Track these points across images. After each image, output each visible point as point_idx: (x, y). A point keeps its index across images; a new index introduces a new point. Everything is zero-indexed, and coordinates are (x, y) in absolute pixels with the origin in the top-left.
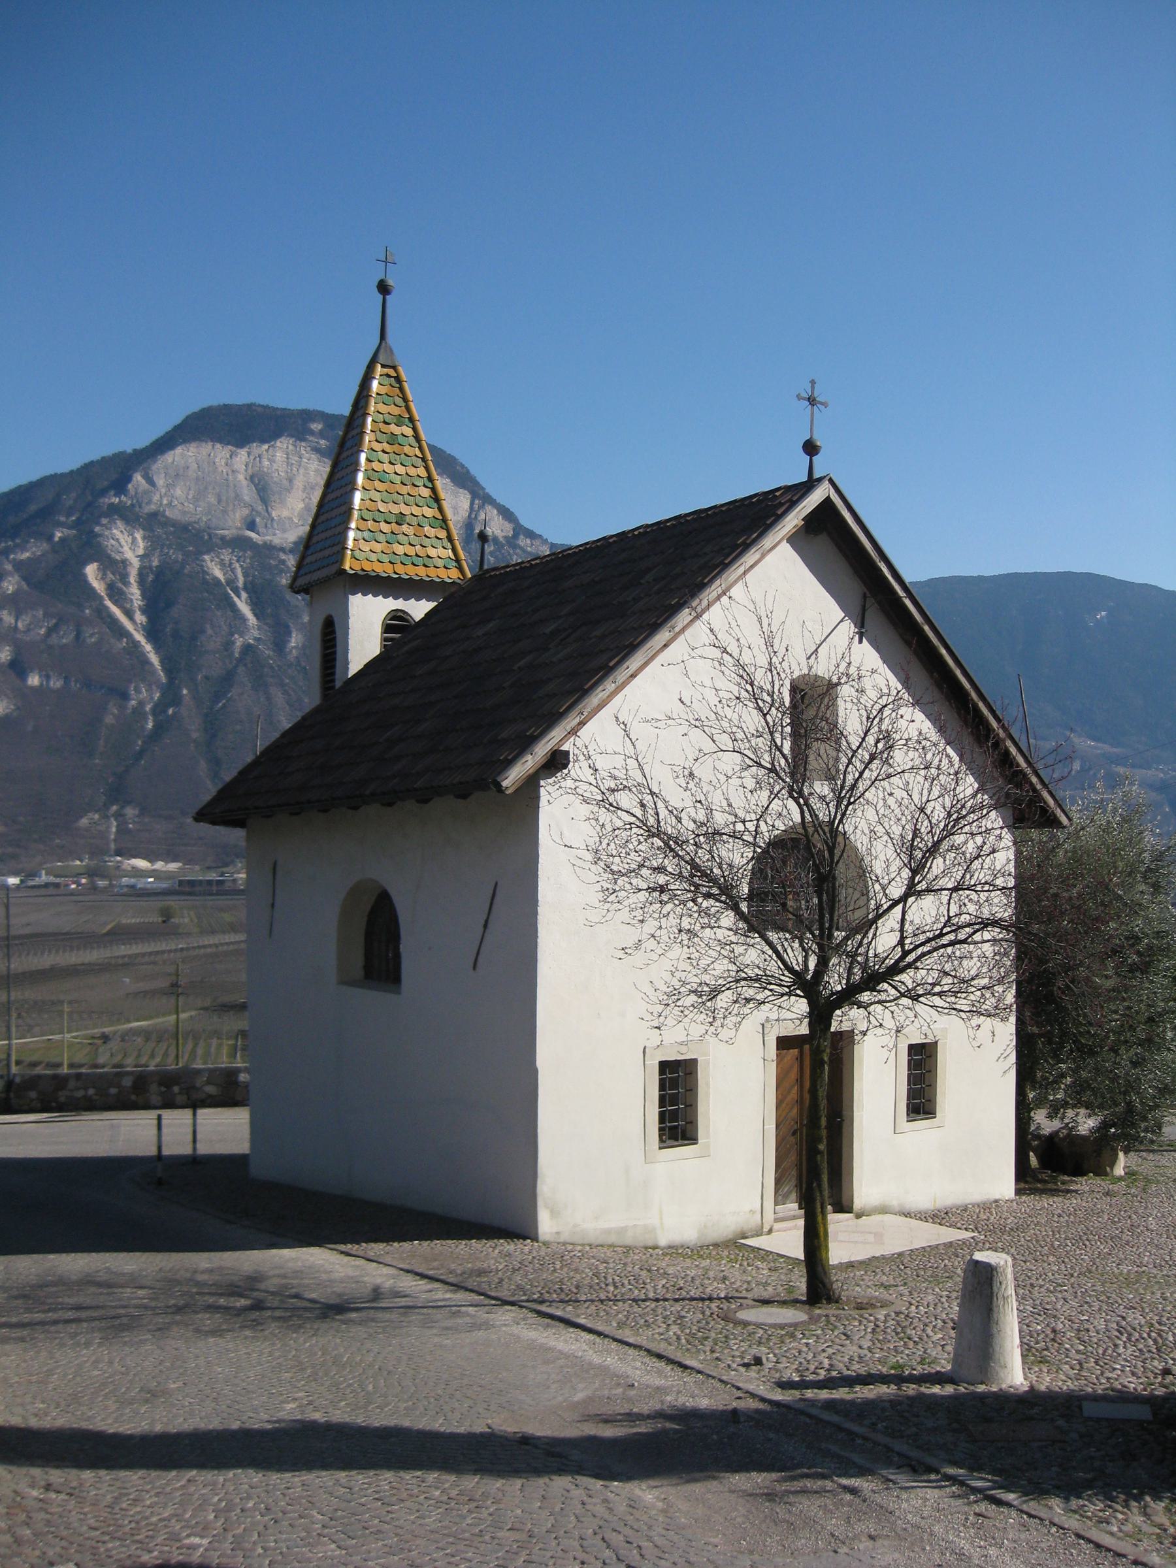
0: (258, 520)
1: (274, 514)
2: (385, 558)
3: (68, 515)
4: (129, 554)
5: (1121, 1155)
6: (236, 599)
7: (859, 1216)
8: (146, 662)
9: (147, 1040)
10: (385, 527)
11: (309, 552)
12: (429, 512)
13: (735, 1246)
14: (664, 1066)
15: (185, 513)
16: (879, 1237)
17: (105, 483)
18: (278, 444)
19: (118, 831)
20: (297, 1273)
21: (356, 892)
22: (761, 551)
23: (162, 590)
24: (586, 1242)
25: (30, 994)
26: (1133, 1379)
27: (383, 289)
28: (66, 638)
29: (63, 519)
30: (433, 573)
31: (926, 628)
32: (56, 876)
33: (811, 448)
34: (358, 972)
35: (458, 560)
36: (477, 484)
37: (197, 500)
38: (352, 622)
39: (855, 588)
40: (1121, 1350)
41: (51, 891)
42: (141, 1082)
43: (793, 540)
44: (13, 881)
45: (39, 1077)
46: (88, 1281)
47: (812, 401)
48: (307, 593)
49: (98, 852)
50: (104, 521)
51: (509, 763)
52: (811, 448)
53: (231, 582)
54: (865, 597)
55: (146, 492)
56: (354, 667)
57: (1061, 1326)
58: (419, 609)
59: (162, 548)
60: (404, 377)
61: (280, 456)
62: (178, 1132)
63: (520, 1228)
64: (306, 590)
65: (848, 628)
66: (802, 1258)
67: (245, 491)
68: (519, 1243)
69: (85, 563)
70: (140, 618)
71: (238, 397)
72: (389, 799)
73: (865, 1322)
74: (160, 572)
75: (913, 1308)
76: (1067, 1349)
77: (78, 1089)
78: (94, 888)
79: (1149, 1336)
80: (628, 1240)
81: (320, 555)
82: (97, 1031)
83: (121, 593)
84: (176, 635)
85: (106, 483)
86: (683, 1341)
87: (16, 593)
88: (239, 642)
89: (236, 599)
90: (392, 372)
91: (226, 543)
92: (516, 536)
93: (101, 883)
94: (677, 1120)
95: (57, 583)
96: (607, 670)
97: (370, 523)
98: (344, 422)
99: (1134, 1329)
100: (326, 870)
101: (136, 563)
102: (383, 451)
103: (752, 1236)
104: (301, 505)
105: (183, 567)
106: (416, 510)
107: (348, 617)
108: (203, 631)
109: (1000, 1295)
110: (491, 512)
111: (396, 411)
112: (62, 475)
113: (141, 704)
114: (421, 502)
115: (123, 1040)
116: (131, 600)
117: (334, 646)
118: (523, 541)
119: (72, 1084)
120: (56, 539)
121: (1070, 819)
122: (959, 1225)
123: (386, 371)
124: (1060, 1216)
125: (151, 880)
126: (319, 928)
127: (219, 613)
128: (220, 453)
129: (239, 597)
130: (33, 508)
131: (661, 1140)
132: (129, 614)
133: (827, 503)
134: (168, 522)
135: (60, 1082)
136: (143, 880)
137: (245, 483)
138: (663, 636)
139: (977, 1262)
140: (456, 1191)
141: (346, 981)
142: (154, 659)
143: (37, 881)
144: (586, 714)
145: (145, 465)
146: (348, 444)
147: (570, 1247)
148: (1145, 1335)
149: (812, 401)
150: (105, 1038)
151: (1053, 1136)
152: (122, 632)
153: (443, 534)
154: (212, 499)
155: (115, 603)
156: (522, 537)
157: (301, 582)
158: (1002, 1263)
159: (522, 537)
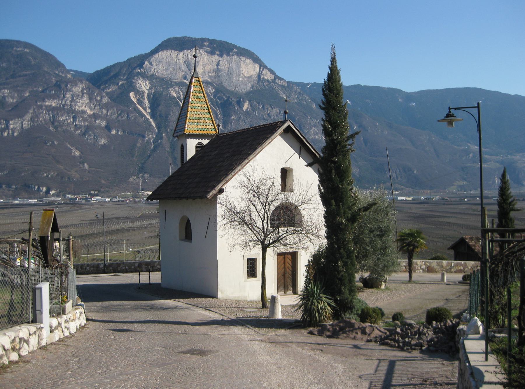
2: (196, 129)
3: (124, 76)
4: (144, 89)
8: (151, 125)
9: (152, 252)
10: (196, 121)
12: (207, 116)
14: (249, 260)
15: (162, 74)
17: (136, 65)
20: (162, 304)
21: (183, 218)
25: (114, 237)
28: (124, 117)
29: (122, 77)
30: (208, 132)
32: (122, 198)
34: (184, 237)
35: (215, 129)
36: (261, 62)
39: (298, 145)
41: (121, 202)
42: (140, 264)
43: (281, 135)
44: (108, 200)
45: (113, 263)
46: (118, 305)
49: (136, 189)
50: (136, 78)
51: (209, 192)
53: (179, 97)
55: (150, 68)
56: (188, 159)
58: (205, 142)
62: (144, 278)
63: (213, 295)
65: (297, 155)
67: (183, 66)
68: (213, 299)
69: (130, 93)
70: (148, 110)
71: (180, 34)
72: (187, 198)
74: (155, 95)
78: (135, 202)
80: (240, 299)
82: (136, 250)
83: (142, 102)
84: (160, 116)
85: (136, 65)
87: (107, 103)
90: (197, 79)
91: (177, 84)
92: (275, 79)
93: (137, 200)
95: (121, 99)
96: (233, 170)
100: (177, 212)
101: (147, 92)
104: (202, 71)
105: (162, 93)
106: (204, 116)
108: (170, 114)
110: (266, 72)
111: (199, 90)
112: (122, 63)
113: (149, 139)
114: (205, 114)
115: (144, 252)
118: (278, 81)
119: (122, 265)
126: (175, 228)
127: (175, 108)
128: (174, 54)
130: (112, 74)
132: (145, 109)
134: (157, 78)
135: (118, 265)
137: (183, 64)
138: (246, 161)
140: (203, 289)
141: (181, 240)
142: (153, 124)
143: (116, 200)
150: (139, 252)
152: (142, 115)
154: (172, 69)
155: (140, 105)
157: (175, 135)
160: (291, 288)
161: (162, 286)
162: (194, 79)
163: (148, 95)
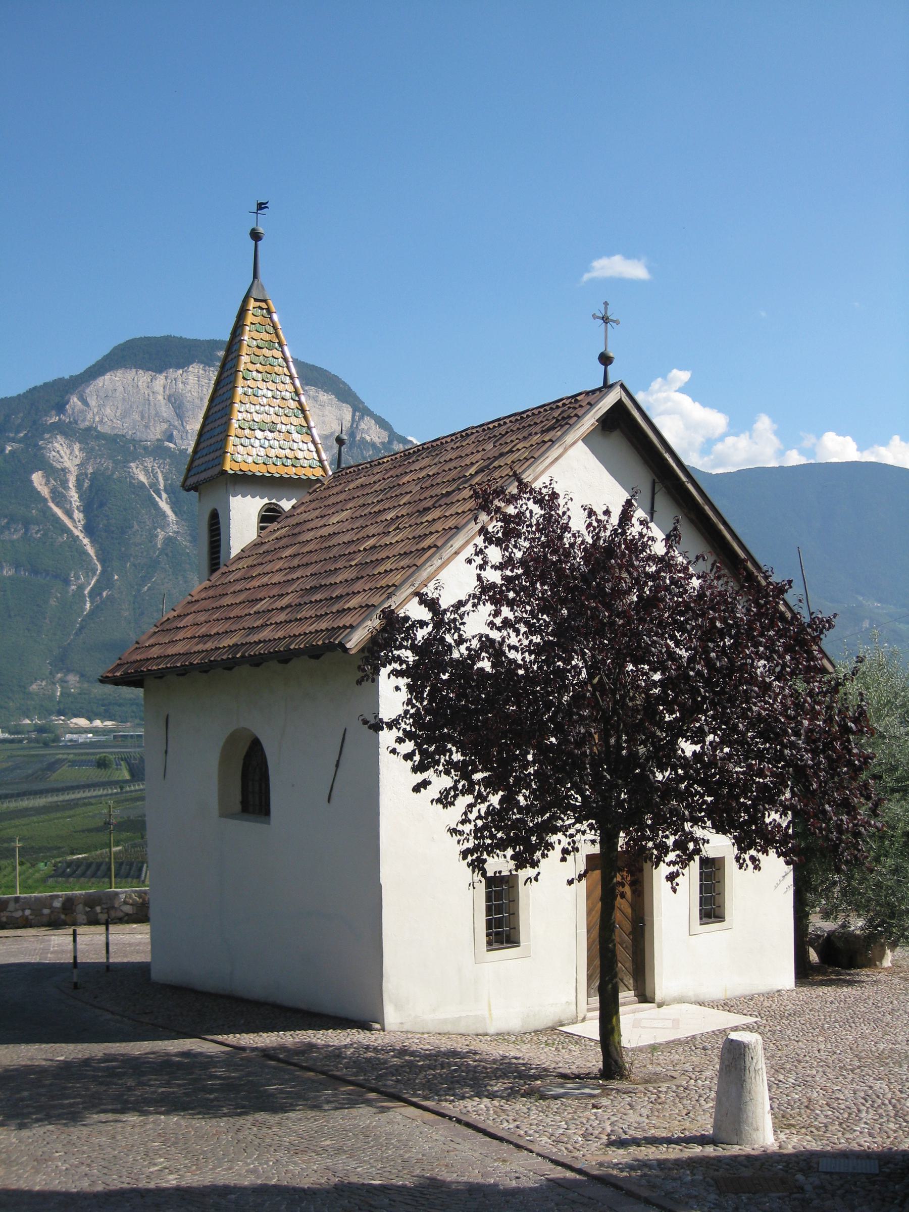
0: (175, 433)
1: (188, 428)
3: (18, 432)
4: (68, 464)
5: (888, 951)
6: (157, 499)
7: (660, 1006)
10: (259, 434)
11: (197, 457)
13: (553, 1032)
16: (676, 1023)
18: (191, 369)
19: (61, 694)
21: (232, 740)
22: (564, 446)
23: (97, 496)
24: (425, 1031)
26: (869, 1139)
27: (256, 236)
31: (706, 508)
32: (10, 733)
33: (605, 359)
34: (238, 807)
35: (321, 461)
37: (124, 417)
38: (233, 514)
40: (863, 1115)
43: (586, 440)
47: (606, 320)
48: (196, 491)
50: (47, 436)
52: (605, 359)
53: (154, 485)
54: (654, 483)
55: (82, 412)
56: (235, 551)
57: (816, 1094)
59: (95, 458)
60: (273, 309)
61: (192, 379)
64: (195, 488)
66: (598, 1038)
70: (78, 515)
73: (649, 1094)
74: (94, 477)
75: (692, 1081)
76: (817, 1115)
77: (16, 910)
79: (890, 1103)
81: (207, 459)
86: (492, 1112)
88: (161, 535)
89: (157, 499)
90: (263, 305)
92: (390, 442)
94: (502, 929)
97: (247, 432)
98: (225, 347)
99: (878, 1097)
102: (258, 371)
103: (569, 1024)
107: (229, 510)
109: (752, 1069)
110: (367, 424)
112: (12, 398)
116: (71, 502)
117: (219, 534)
119: (12, 906)
120: (7, 452)
121: (834, 666)
122: (745, 1012)
123: (258, 304)
124: (832, 1003)
125: (91, 735)
128: (143, 377)
129: (160, 497)
131: (489, 943)
133: (619, 404)
134: (100, 436)
136: (84, 736)
137: (163, 402)
139: (732, 1040)
141: (225, 814)
144: (416, 586)
145: (80, 389)
146: (228, 366)
147: (410, 1036)
148: (887, 1102)
149: (606, 320)
151: (831, 934)
152: (65, 529)
153: (308, 439)
154: (137, 417)
155: (57, 505)
156: (395, 442)
157: (191, 481)
158: (753, 1041)
159: (395, 442)
160: (630, 982)
161: (156, 975)
162: (252, 304)
163: (78, 480)
